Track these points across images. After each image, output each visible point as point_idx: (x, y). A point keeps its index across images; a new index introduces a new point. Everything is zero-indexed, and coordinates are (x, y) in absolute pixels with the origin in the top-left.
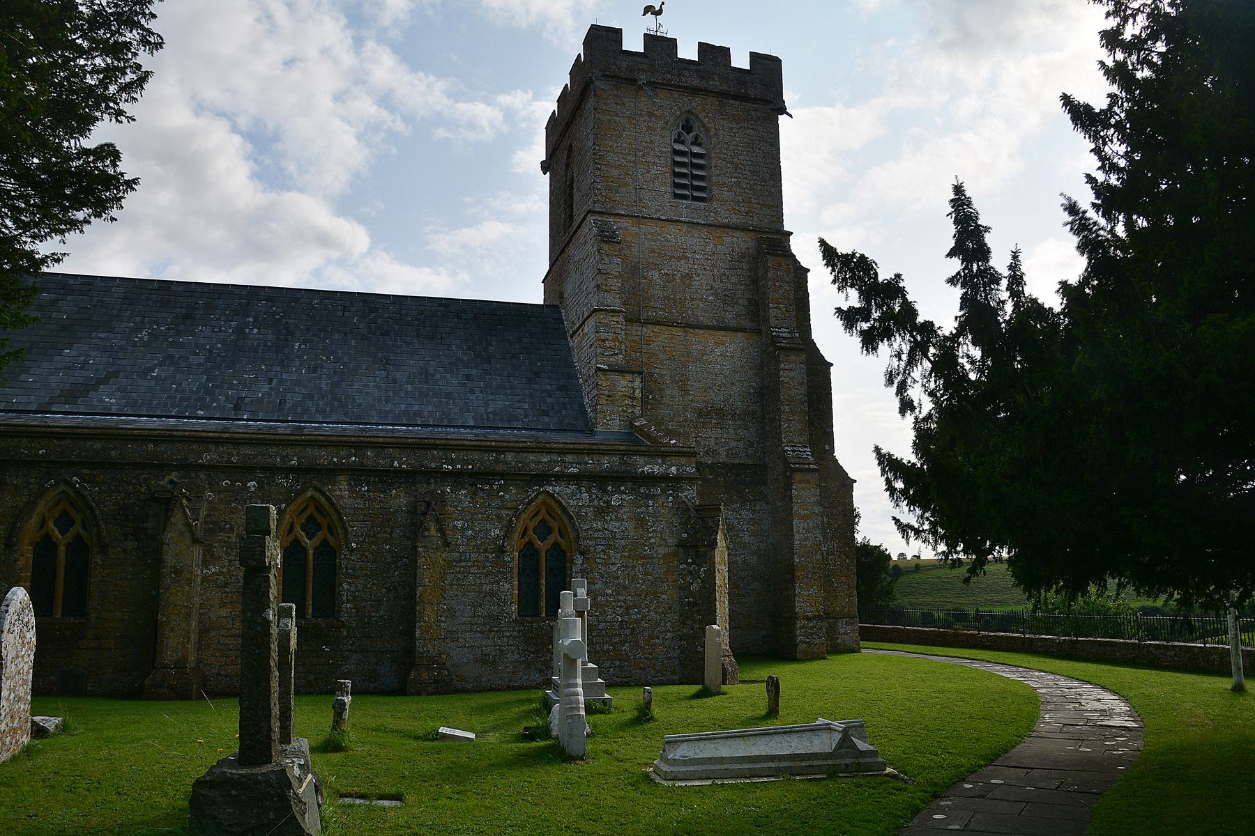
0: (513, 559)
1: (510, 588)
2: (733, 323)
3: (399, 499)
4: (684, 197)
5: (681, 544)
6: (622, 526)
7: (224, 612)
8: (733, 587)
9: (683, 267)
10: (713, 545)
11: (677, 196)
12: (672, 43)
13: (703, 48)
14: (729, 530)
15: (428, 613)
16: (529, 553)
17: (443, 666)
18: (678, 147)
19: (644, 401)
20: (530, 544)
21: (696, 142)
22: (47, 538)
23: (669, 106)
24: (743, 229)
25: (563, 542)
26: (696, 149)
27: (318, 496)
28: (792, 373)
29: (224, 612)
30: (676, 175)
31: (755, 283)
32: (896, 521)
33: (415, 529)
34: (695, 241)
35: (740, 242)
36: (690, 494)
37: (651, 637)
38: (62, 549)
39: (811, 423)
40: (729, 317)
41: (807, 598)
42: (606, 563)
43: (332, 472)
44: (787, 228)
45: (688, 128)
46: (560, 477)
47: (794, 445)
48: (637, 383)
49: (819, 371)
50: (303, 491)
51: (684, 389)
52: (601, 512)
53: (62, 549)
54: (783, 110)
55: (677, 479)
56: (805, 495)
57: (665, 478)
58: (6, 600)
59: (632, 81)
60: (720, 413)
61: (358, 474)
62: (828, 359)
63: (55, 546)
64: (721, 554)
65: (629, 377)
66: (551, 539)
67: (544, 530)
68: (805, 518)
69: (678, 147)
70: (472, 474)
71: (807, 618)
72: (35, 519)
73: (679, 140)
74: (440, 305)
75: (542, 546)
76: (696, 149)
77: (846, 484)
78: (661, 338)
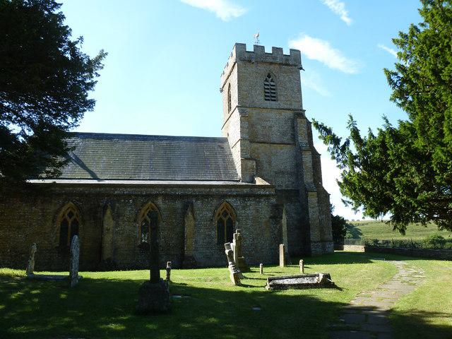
0: (215, 223)
1: (214, 233)
2: (286, 142)
3: (178, 205)
4: (268, 100)
5: (271, 217)
6: (251, 211)
7: (122, 243)
8: (289, 231)
9: (268, 124)
10: (281, 218)
11: (266, 100)
12: (263, 48)
13: (274, 48)
14: (287, 212)
15: (188, 242)
16: (221, 221)
17: (194, 259)
18: (267, 83)
19: (257, 170)
20: (221, 219)
21: (272, 81)
22: (65, 220)
23: (263, 69)
24: (289, 110)
25: (232, 218)
26: (272, 83)
27: (152, 204)
28: (307, 158)
29: (122, 243)
30: (265, 92)
31: (293, 128)
32: (343, 201)
33: (184, 214)
34: (273, 115)
35: (289, 114)
36: (273, 200)
37: (262, 249)
38: (70, 223)
39: (314, 175)
40: (285, 139)
41: (315, 235)
42: (246, 224)
43: (157, 195)
44: (304, 109)
45: (269, 76)
46: (230, 196)
47: (308, 178)
48: (254, 164)
49: (316, 157)
50: (147, 202)
51: (270, 165)
52: (244, 208)
53: (70, 223)
54: (301, 68)
55: (269, 196)
56: (313, 199)
57: (265, 195)
58: (109, 218)
59: (250, 61)
60: (283, 173)
61: (166, 196)
62: (88, 50)
63: (67, 222)
64: (284, 221)
65: (251, 161)
66: (228, 217)
67: (225, 214)
68: (313, 208)
69: (267, 83)
70: (203, 196)
71: (315, 242)
72: (61, 215)
73: (266, 80)
74: (195, 141)
75: (225, 219)
76: (272, 83)
77: (327, 196)
78: (262, 147)
